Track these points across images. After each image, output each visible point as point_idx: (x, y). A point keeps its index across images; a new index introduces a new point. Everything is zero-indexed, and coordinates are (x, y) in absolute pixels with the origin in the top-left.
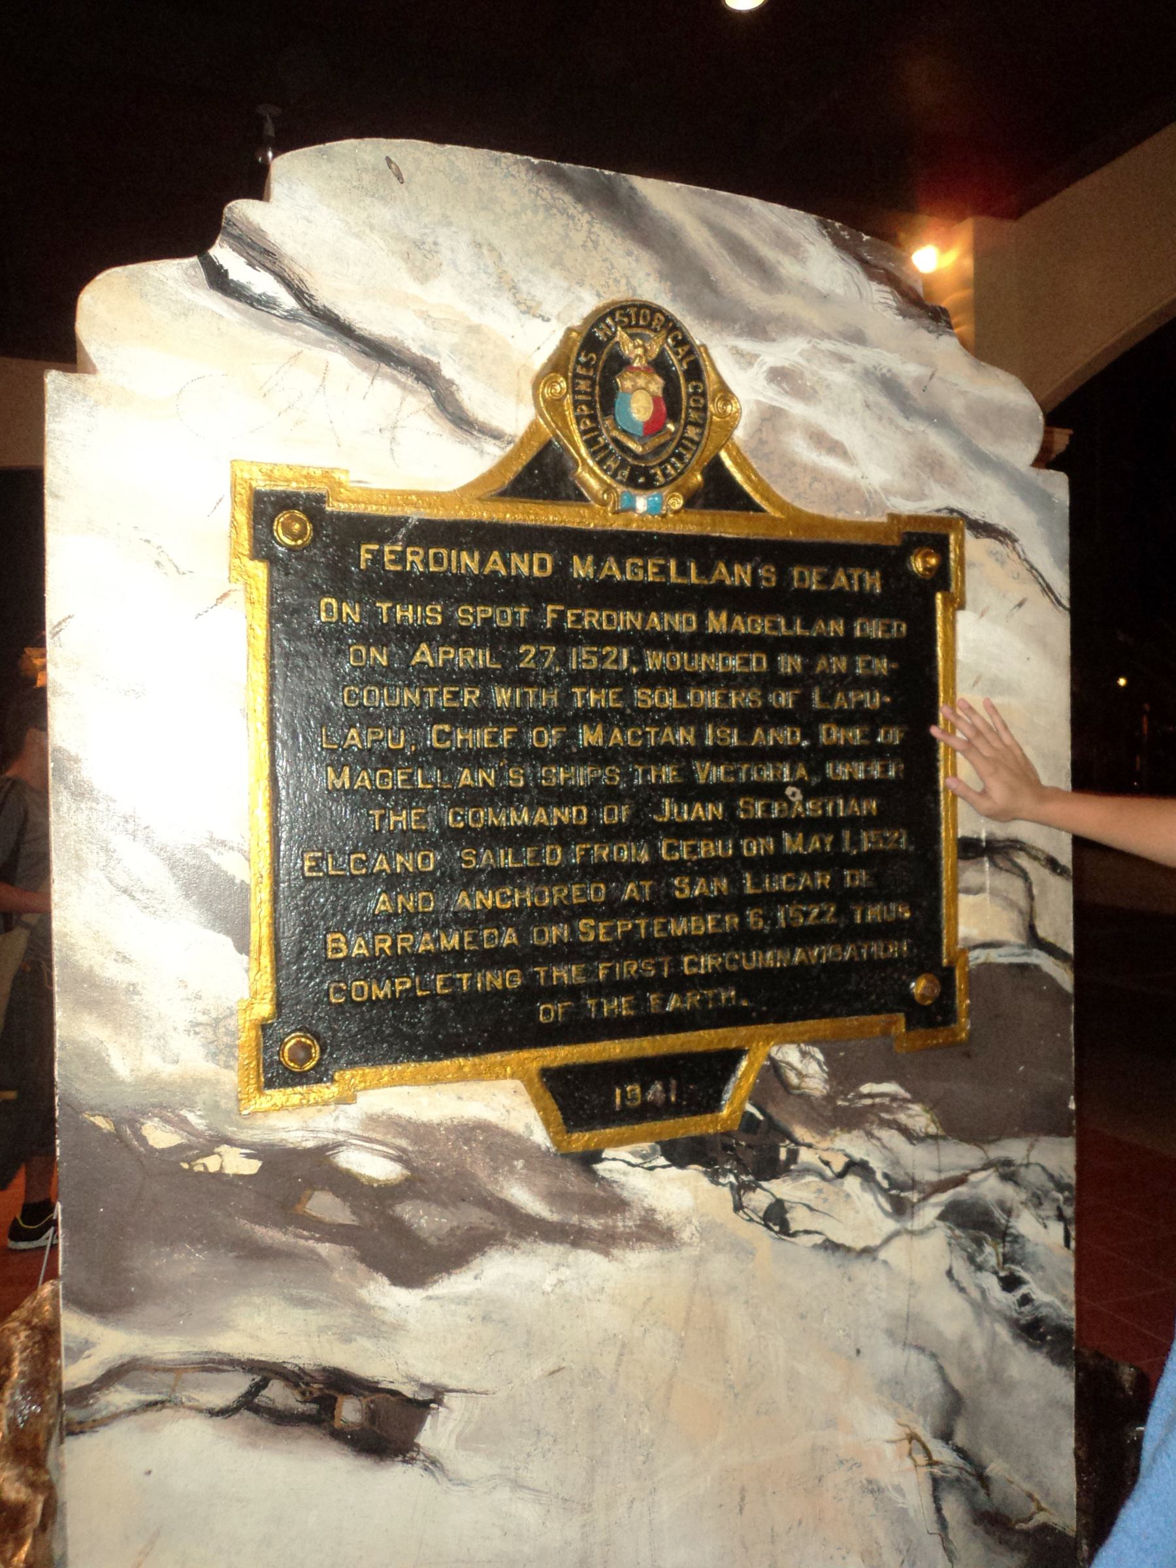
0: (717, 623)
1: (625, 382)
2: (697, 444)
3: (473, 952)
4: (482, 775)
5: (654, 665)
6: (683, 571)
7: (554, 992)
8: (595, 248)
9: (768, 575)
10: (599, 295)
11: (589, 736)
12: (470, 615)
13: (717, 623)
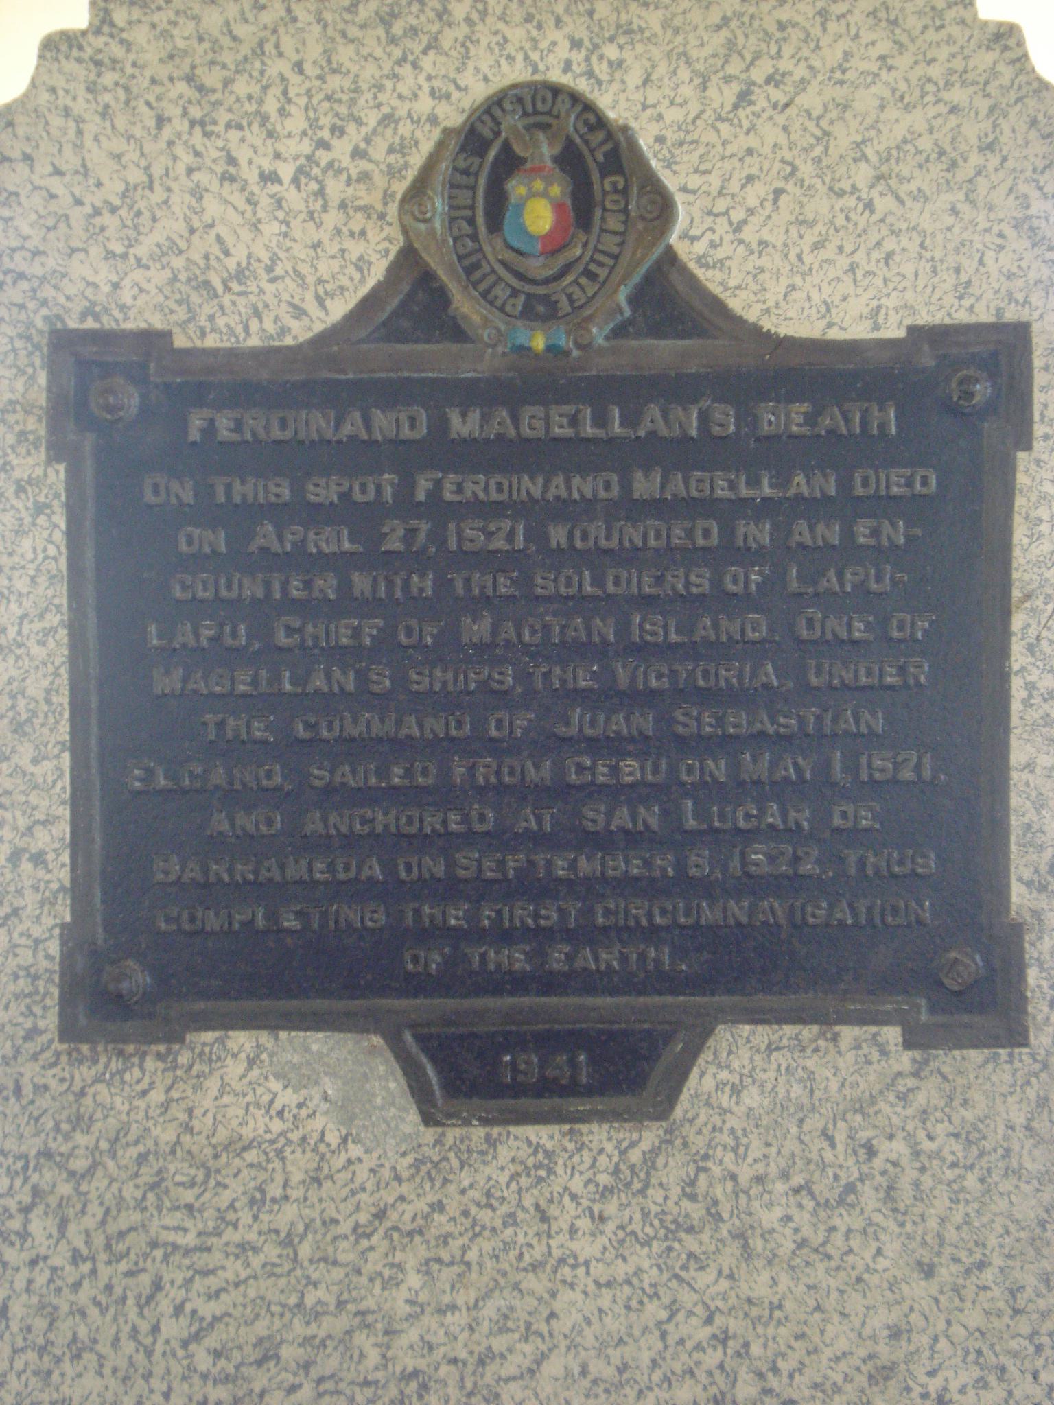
0: (645, 485)
1: (517, 188)
2: (616, 257)
3: (326, 883)
4: (637, 719)
5: (57, 472)
6: (601, 420)
7: (427, 934)
8: (483, 20)
9: (726, 420)
10: (486, 79)
11: (478, 629)
12: (324, 491)
13: (645, 485)
